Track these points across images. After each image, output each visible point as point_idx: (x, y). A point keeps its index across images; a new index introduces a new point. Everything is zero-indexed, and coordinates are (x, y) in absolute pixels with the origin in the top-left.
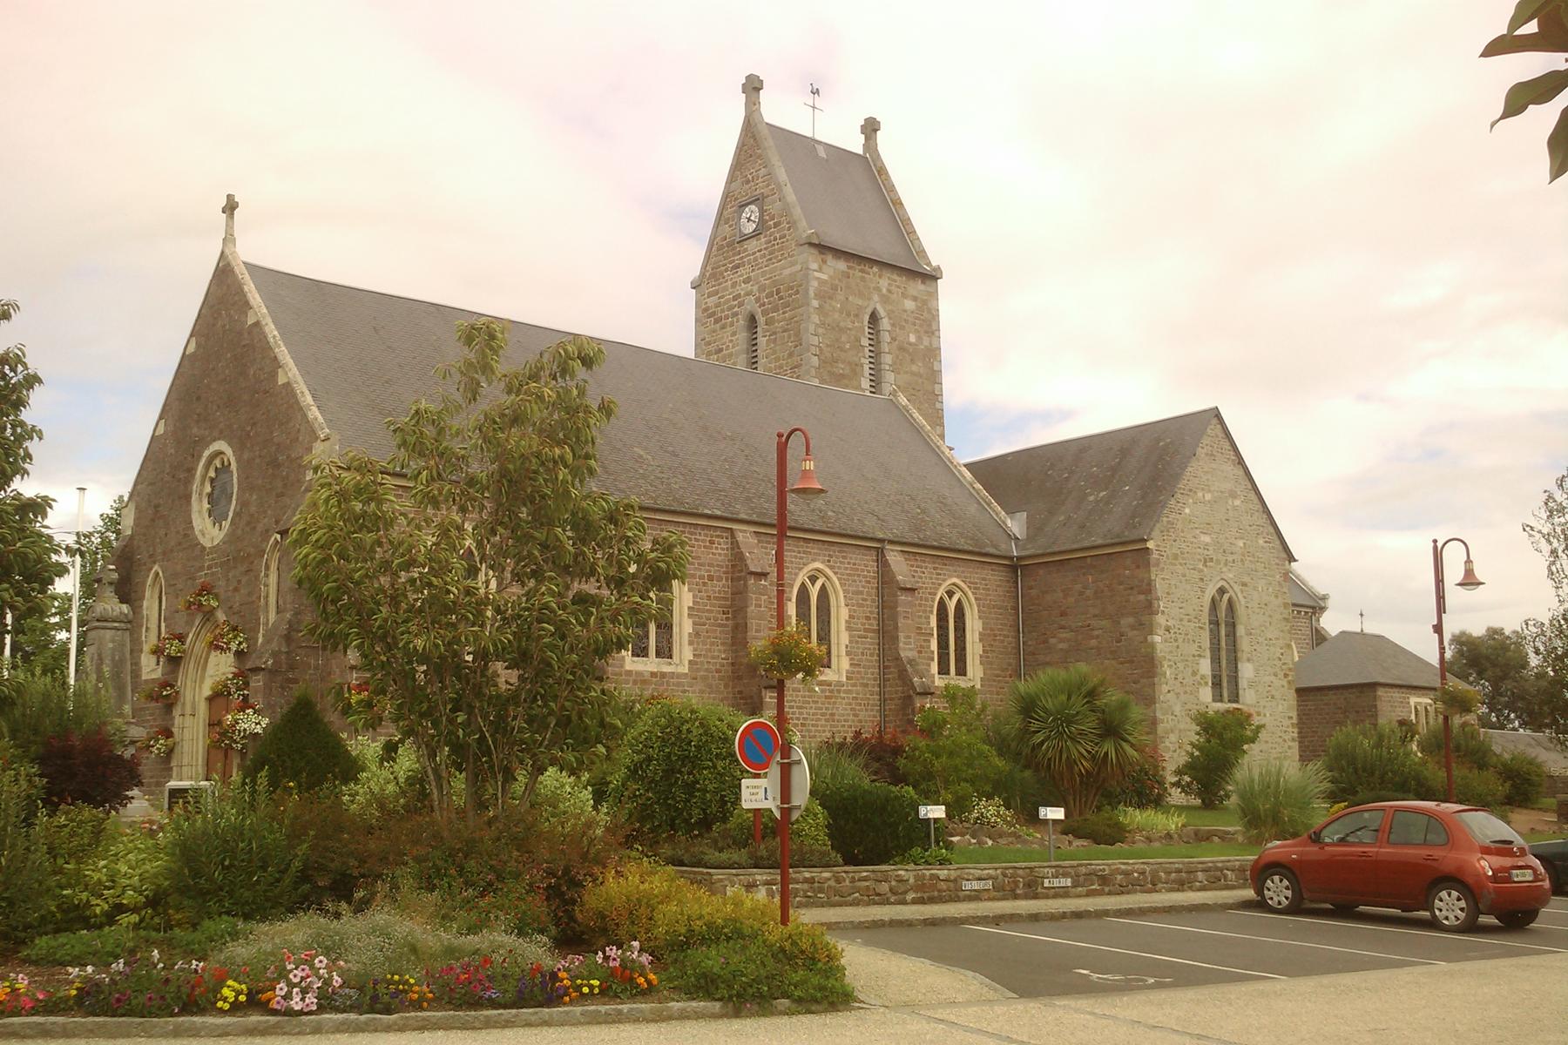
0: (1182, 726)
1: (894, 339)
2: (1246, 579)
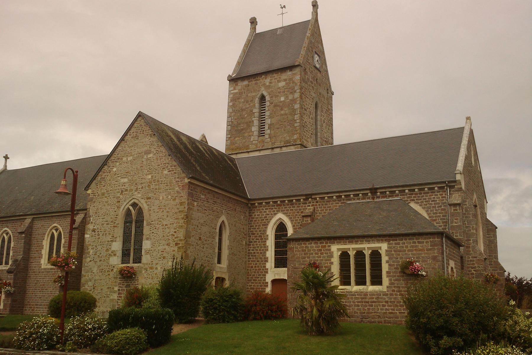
0: (97, 278)
1: (271, 103)
2: (150, 195)
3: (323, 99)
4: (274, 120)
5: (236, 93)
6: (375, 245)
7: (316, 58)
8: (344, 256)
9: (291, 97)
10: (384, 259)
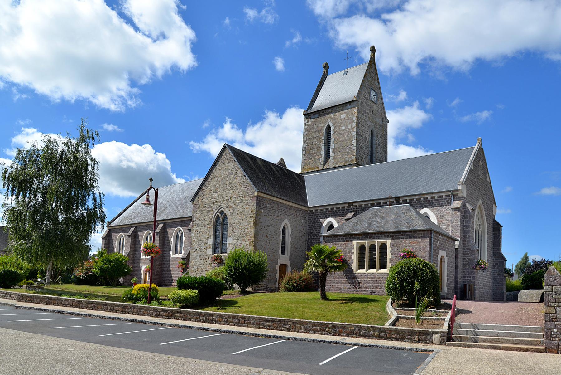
3: (378, 127)
4: (337, 146)
5: (310, 125)
6: (382, 240)
7: (373, 93)
8: (362, 249)
9: (350, 126)
10: (389, 249)
